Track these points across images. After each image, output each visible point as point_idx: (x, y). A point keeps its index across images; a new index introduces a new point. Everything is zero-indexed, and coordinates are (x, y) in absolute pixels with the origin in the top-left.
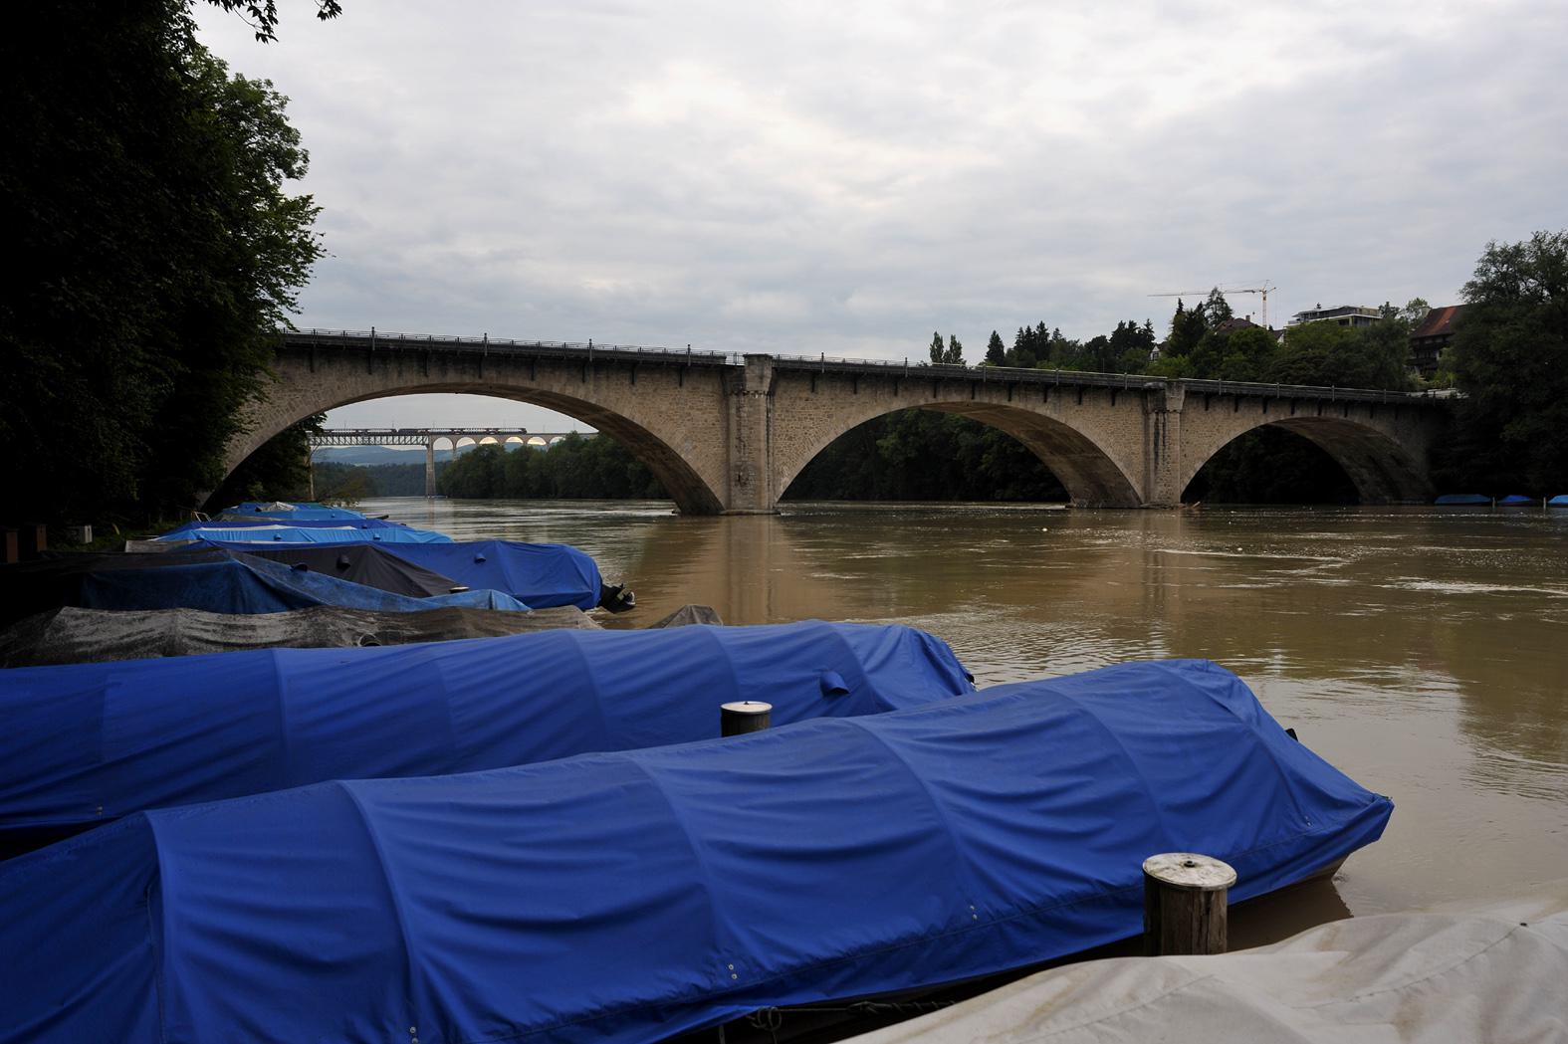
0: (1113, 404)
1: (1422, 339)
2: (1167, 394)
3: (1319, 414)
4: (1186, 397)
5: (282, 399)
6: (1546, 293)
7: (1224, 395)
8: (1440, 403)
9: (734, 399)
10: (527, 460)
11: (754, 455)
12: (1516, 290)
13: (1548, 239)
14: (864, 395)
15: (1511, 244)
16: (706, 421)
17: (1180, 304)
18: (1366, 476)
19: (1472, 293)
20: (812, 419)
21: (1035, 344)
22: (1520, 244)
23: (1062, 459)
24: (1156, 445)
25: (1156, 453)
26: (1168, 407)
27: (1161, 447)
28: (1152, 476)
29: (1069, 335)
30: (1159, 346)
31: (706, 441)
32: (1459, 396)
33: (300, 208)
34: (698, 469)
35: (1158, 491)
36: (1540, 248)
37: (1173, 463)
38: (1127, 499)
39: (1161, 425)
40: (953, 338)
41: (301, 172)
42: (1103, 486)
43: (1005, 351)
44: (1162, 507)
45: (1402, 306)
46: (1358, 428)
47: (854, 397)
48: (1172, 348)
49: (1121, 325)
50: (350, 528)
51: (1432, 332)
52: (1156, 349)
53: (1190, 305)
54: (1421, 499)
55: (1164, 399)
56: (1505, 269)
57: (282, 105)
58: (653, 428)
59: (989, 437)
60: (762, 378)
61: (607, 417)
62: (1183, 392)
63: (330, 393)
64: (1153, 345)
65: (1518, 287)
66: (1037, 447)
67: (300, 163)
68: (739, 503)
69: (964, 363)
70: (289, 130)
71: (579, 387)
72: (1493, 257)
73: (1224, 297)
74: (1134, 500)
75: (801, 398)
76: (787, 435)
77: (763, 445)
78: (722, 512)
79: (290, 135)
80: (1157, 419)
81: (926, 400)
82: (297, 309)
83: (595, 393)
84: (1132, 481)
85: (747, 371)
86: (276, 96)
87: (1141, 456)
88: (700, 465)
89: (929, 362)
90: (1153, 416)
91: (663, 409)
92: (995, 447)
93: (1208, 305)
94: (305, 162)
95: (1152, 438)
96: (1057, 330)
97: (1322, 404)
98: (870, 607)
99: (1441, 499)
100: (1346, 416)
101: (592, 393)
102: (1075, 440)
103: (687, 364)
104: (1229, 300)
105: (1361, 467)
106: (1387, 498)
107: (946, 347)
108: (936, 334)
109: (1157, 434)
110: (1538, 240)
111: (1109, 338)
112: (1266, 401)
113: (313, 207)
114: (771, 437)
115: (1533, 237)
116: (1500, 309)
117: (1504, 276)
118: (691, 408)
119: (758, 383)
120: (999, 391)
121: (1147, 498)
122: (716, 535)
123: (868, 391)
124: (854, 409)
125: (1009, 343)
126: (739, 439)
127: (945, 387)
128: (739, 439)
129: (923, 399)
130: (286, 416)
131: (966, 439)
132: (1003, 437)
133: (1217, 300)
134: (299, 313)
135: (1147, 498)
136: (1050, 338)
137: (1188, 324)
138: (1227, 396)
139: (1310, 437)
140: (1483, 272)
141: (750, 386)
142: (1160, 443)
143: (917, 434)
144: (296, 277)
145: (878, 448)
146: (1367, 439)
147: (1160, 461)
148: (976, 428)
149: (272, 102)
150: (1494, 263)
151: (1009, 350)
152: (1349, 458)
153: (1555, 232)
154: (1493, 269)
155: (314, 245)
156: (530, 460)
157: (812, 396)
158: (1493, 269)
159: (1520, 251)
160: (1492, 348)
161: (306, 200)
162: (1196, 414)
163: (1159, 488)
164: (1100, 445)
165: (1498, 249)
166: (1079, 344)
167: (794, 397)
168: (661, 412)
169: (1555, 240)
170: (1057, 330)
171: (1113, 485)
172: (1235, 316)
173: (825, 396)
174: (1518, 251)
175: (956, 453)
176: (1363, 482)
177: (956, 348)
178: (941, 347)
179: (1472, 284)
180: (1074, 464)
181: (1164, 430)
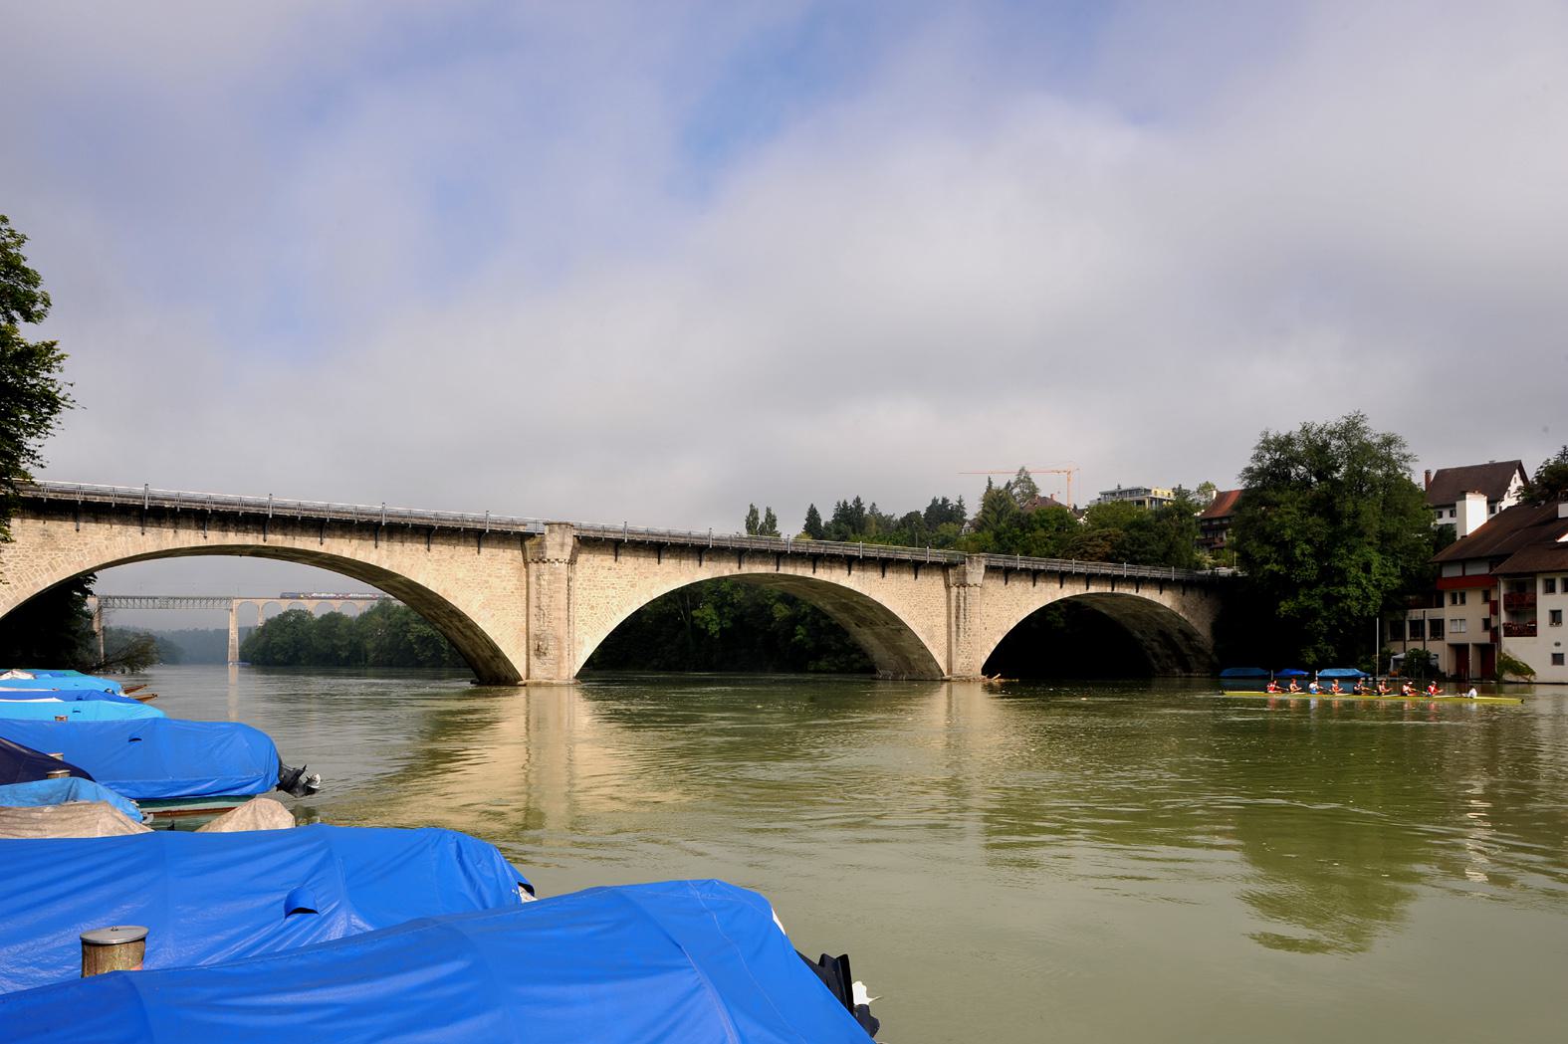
0: (883, 576)
1: (1210, 520)
2: (968, 568)
3: (1113, 589)
4: (986, 571)
5: (42, 558)
6: (1314, 479)
7: (1022, 569)
8: (1224, 579)
9: (533, 567)
10: (336, 627)
11: (554, 623)
12: (1288, 476)
13: (1315, 429)
14: (669, 564)
15: (1284, 433)
16: (505, 589)
17: (990, 483)
18: (1158, 650)
19: (1251, 478)
20: (615, 588)
21: (852, 520)
22: (1290, 433)
23: (866, 631)
24: (957, 617)
25: (958, 626)
26: (969, 580)
27: (962, 620)
28: (954, 648)
29: (885, 510)
30: (969, 522)
31: (504, 609)
32: (1240, 574)
33: (39, 356)
34: (496, 638)
35: (960, 664)
36: (1308, 438)
37: (974, 635)
38: (929, 670)
39: (962, 599)
40: (768, 510)
41: (40, 315)
42: (907, 658)
43: (823, 524)
44: (966, 680)
45: (1193, 488)
46: (1149, 603)
47: (658, 567)
48: (980, 525)
49: (935, 501)
50: (54, 700)
51: (1218, 513)
52: (967, 525)
53: (999, 484)
54: (1207, 672)
55: (964, 574)
56: (1278, 457)
57: (20, 243)
58: (449, 595)
59: (804, 609)
60: (562, 545)
61: (400, 582)
62: (983, 566)
63: (97, 553)
64: (965, 521)
65: (1290, 473)
66: (841, 617)
67: (39, 307)
68: (539, 673)
69: (779, 535)
70: (25, 271)
71: (371, 552)
72: (1267, 445)
73: (1031, 476)
74: (937, 672)
75: (603, 567)
76: (588, 605)
77: (563, 615)
78: (520, 683)
79: (31, 278)
80: (959, 593)
81: (731, 571)
82: (40, 463)
83: (388, 558)
84: (935, 653)
85: (548, 538)
86: (12, 234)
87: (944, 630)
88: (498, 633)
89: (744, 533)
90: (954, 590)
91: (460, 575)
92: (809, 619)
93: (1016, 484)
94: (46, 306)
95: (953, 611)
96: (874, 504)
97: (1114, 580)
98: (1030, 787)
99: (1226, 672)
100: (1137, 591)
101: (385, 558)
102: (879, 612)
103: (268, 515)
104: (1036, 479)
105: (1153, 640)
106: (1177, 670)
107: (762, 519)
108: (751, 506)
109: (958, 607)
110: (1305, 430)
111: (923, 512)
112: (1063, 577)
113: (57, 354)
114: (571, 606)
115: (1301, 428)
116: (1274, 493)
117: (1277, 463)
118: (490, 576)
119: (558, 547)
120: (804, 563)
121: (950, 671)
122: (510, 709)
123: (672, 561)
124: (658, 579)
125: (827, 516)
126: (539, 607)
127: (750, 557)
128: (539, 607)
129: (727, 569)
130: (45, 576)
131: (781, 611)
132: (815, 610)
133: (1024, 479)
134: (42, 466)
135: (950, 671)
136: (866, 512)
137: (996, 501)
138: (1025, 571)
139: (1104, 611)
140: (1258, 458)
141: (550, 554)
142: (962, 616)
143: (732, 605)
144: (39, 425)
145: (693, 618)
146: (1158, 614)
147: (962, 634)
148: (788, 599)
149: (8, 240)
150: (1268, 450)
151: (826, 523)
152: (1142, 632)
153: (1320, 423)
154: (1268, 456)
155: (60, 395)
156: (339, 626)
157: (614, 565)
158: (1268, 456)
159: (1291, 440)
160: (1268, 529)
161: (50, 347)
162: (996, 586)
163: (961, 660)
164: (903, 617)
165: (1271, 438)
166: (894, 519)
167: (595, 564)
168: (457, 579)
169: (1321, 431)
170: (874, 504)
171: (916, 657)
172: (1041, 494)
173: (629, 563)
174: (1289, 440)
175: (770, 624)
176: (1156, 656)
177: (771, 520)
178: (756, 518)
179: (1249, 470)
180: (878, 636)
181: (965, 603)
